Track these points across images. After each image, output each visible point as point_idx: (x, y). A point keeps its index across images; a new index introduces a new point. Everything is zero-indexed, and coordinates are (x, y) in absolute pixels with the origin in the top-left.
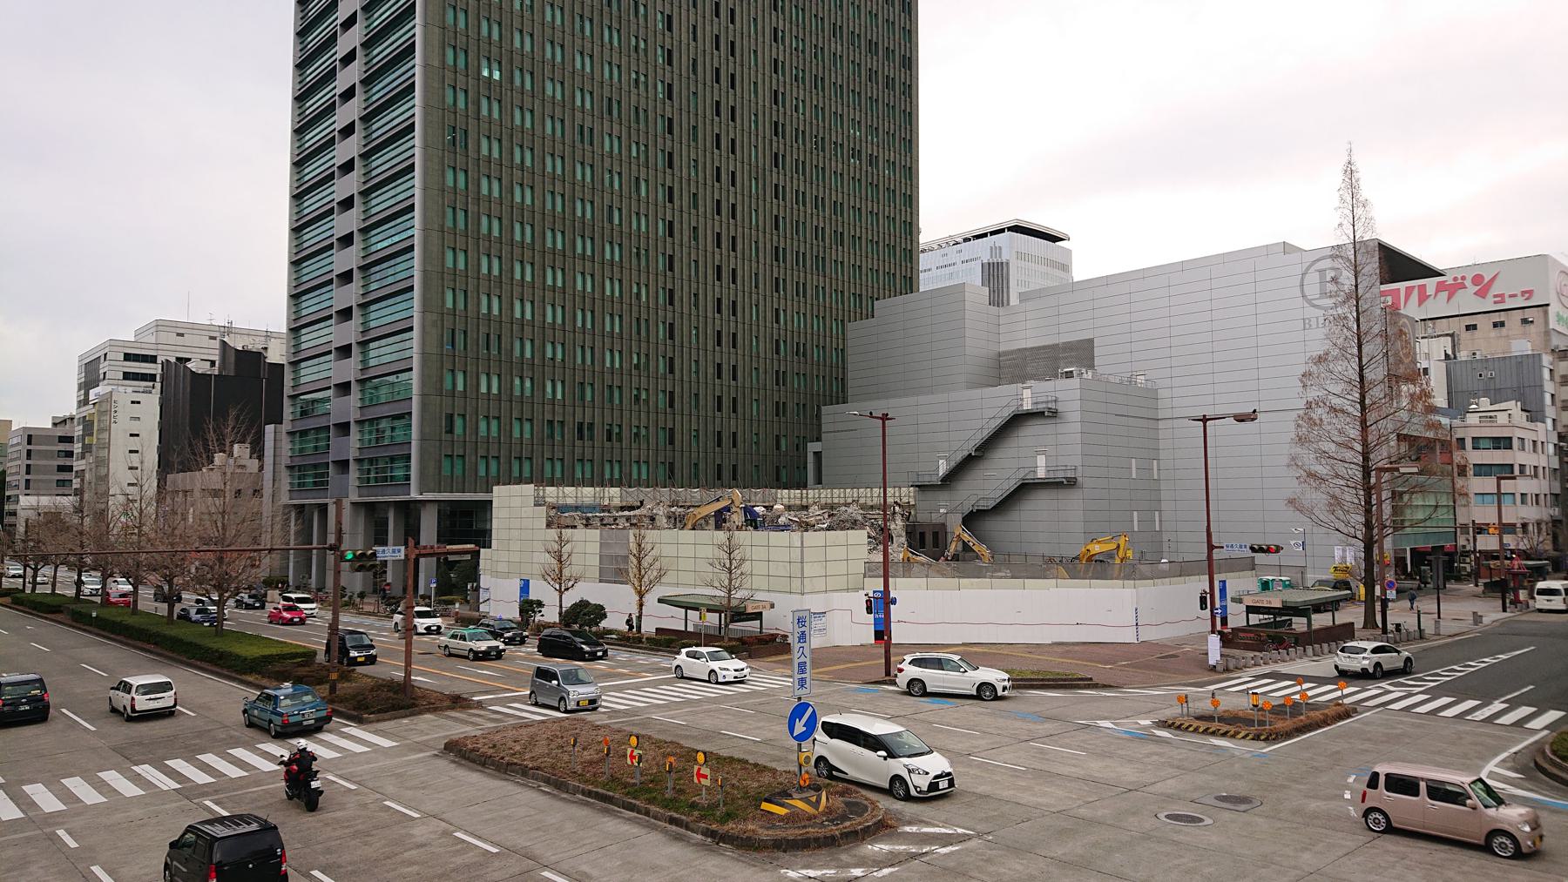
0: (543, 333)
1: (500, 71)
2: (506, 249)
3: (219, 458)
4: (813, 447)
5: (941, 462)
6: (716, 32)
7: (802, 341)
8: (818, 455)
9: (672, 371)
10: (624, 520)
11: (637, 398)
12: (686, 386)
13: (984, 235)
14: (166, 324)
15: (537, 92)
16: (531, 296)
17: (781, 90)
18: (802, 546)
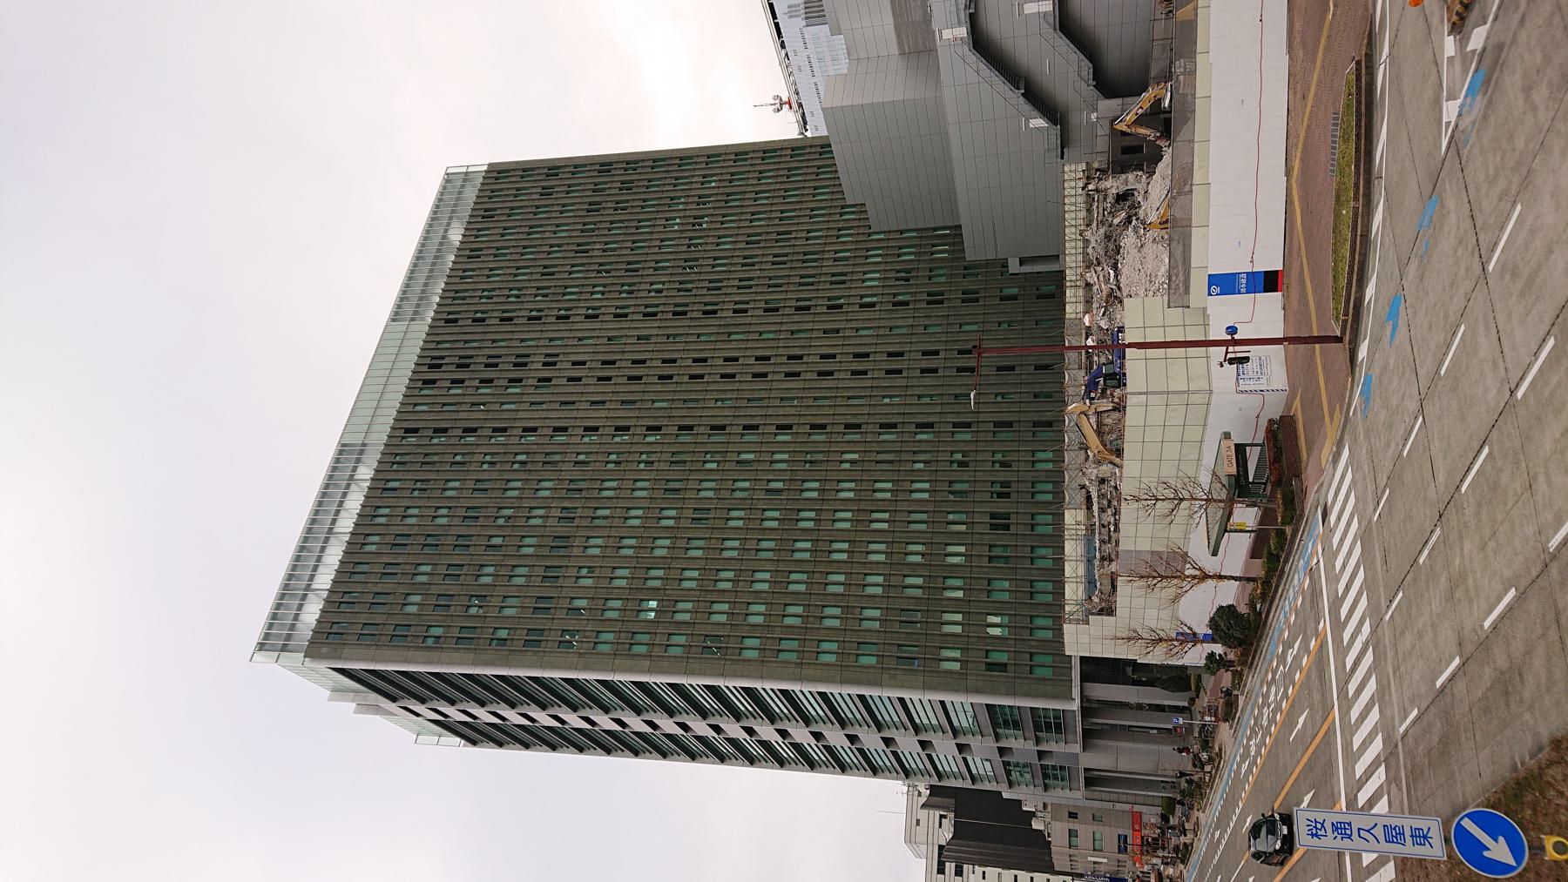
0: (896, 566)
1: (649, 600)
2: (814, 601)
3: (1037, 825)
4: (1014, 266)
5: (1031, 126)
6: (594, 381)
7: (894, 275)
8: (1022, 262)
9: (931, 425)
10: (1104, 516)
11: (961, 464)
12: (947, 409)
13: (777, 25)
14: (910, 805)
15: (666, 566)
16: (878, 399)
17: (642, 309)
18: (1146, 393)
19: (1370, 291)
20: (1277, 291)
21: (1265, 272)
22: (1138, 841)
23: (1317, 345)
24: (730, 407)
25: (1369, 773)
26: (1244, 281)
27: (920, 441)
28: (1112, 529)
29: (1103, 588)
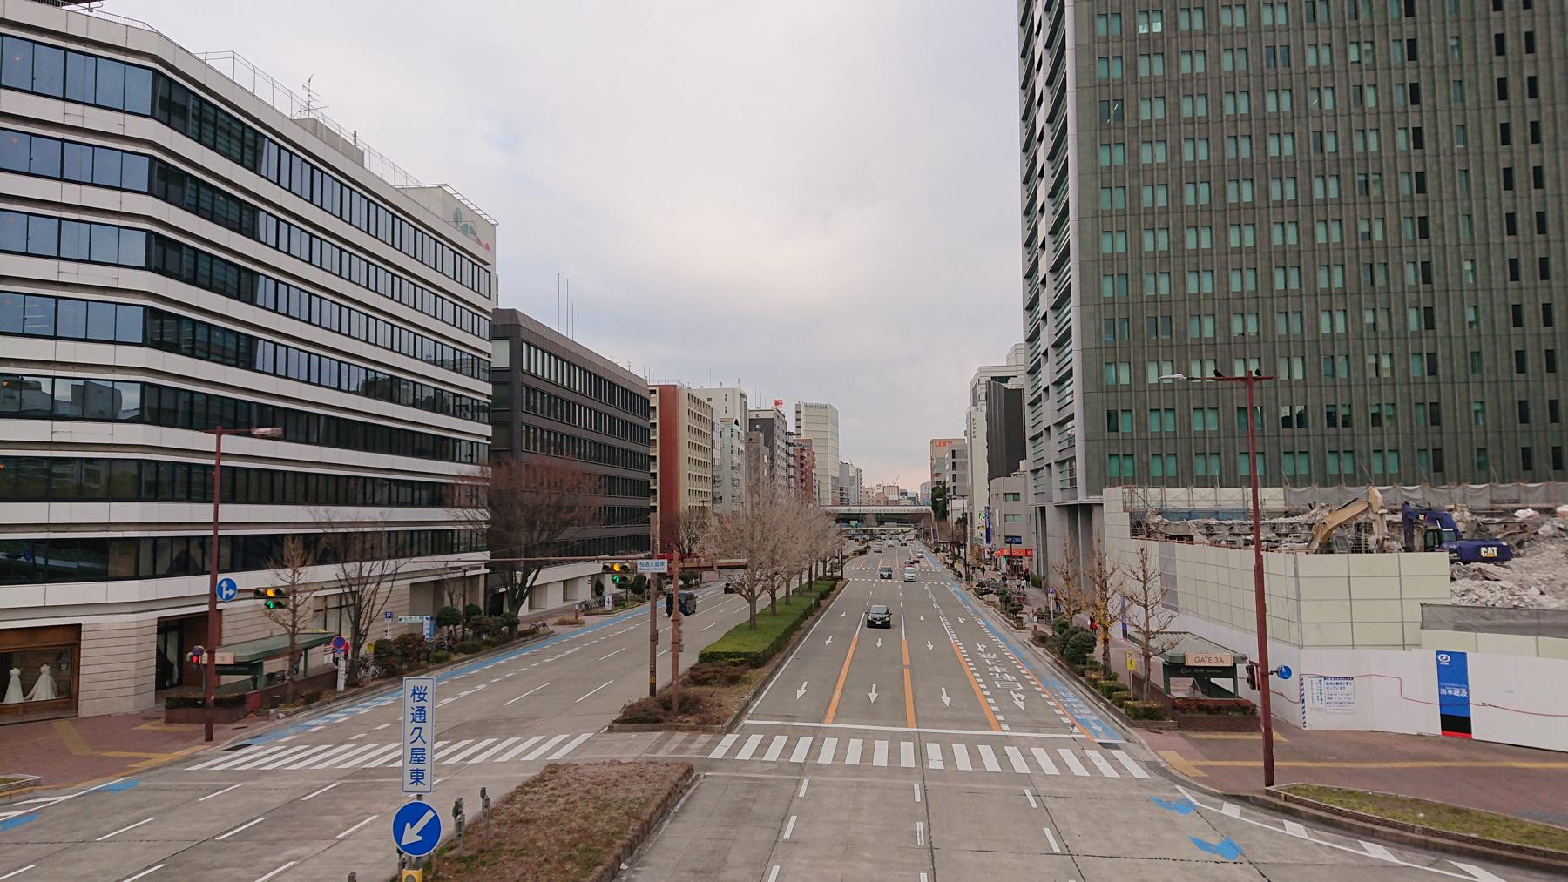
0: (1226, 305)
20: (1443, 728)
21: (1468, 719)
22: (1015, 553)
23: (1275, 763)
24: (1447, 59)
26: (1457, 693)
27: (1405, 315)
28: (1248, 538)
29: (1172, 527)
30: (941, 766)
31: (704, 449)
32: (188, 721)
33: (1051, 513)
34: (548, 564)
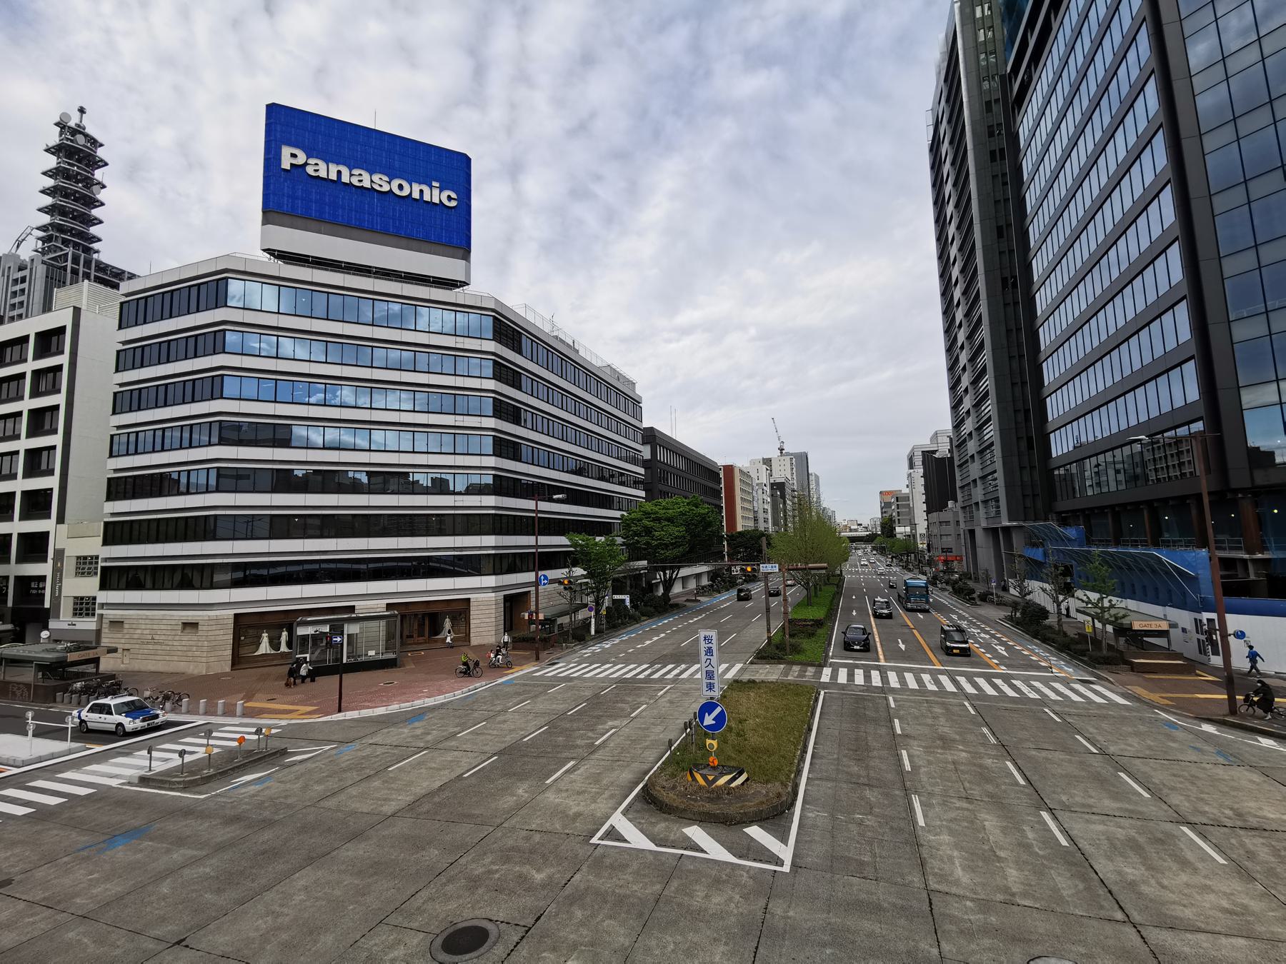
3: (950, 503)
19: (1266, 742)
22: (950, 559)
25: (975, 685)
30: (880, 685)
31: (749, 501)
32: (525, 649)
33: (979, 535)
34: (683, 567)
